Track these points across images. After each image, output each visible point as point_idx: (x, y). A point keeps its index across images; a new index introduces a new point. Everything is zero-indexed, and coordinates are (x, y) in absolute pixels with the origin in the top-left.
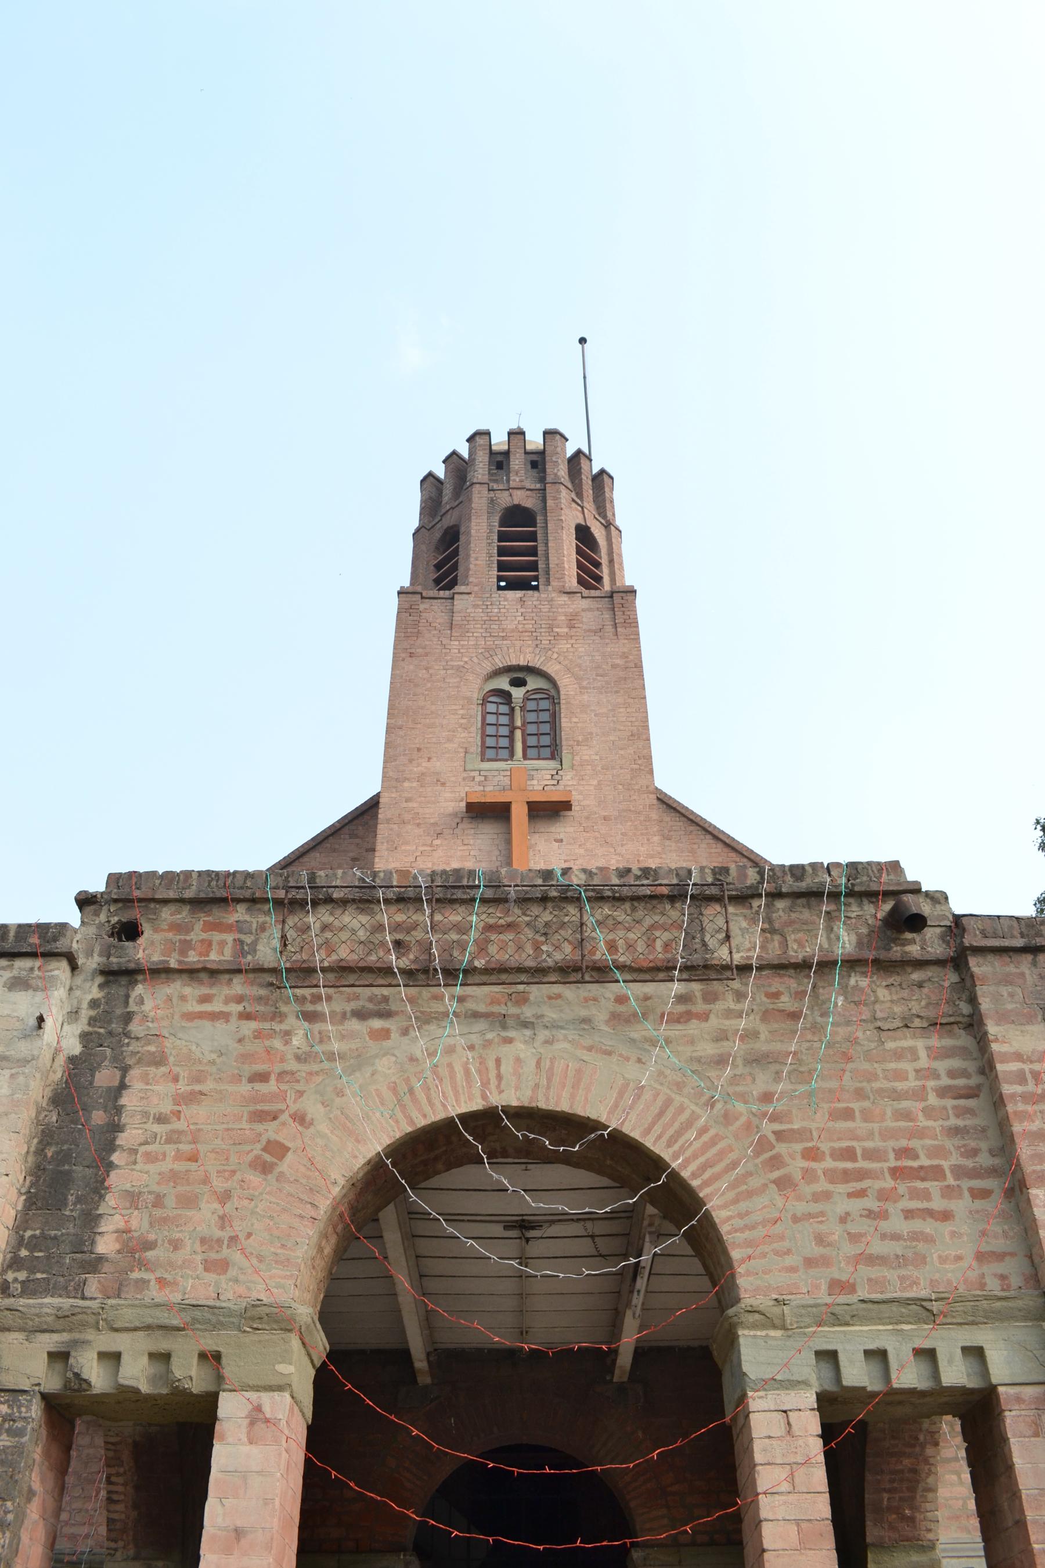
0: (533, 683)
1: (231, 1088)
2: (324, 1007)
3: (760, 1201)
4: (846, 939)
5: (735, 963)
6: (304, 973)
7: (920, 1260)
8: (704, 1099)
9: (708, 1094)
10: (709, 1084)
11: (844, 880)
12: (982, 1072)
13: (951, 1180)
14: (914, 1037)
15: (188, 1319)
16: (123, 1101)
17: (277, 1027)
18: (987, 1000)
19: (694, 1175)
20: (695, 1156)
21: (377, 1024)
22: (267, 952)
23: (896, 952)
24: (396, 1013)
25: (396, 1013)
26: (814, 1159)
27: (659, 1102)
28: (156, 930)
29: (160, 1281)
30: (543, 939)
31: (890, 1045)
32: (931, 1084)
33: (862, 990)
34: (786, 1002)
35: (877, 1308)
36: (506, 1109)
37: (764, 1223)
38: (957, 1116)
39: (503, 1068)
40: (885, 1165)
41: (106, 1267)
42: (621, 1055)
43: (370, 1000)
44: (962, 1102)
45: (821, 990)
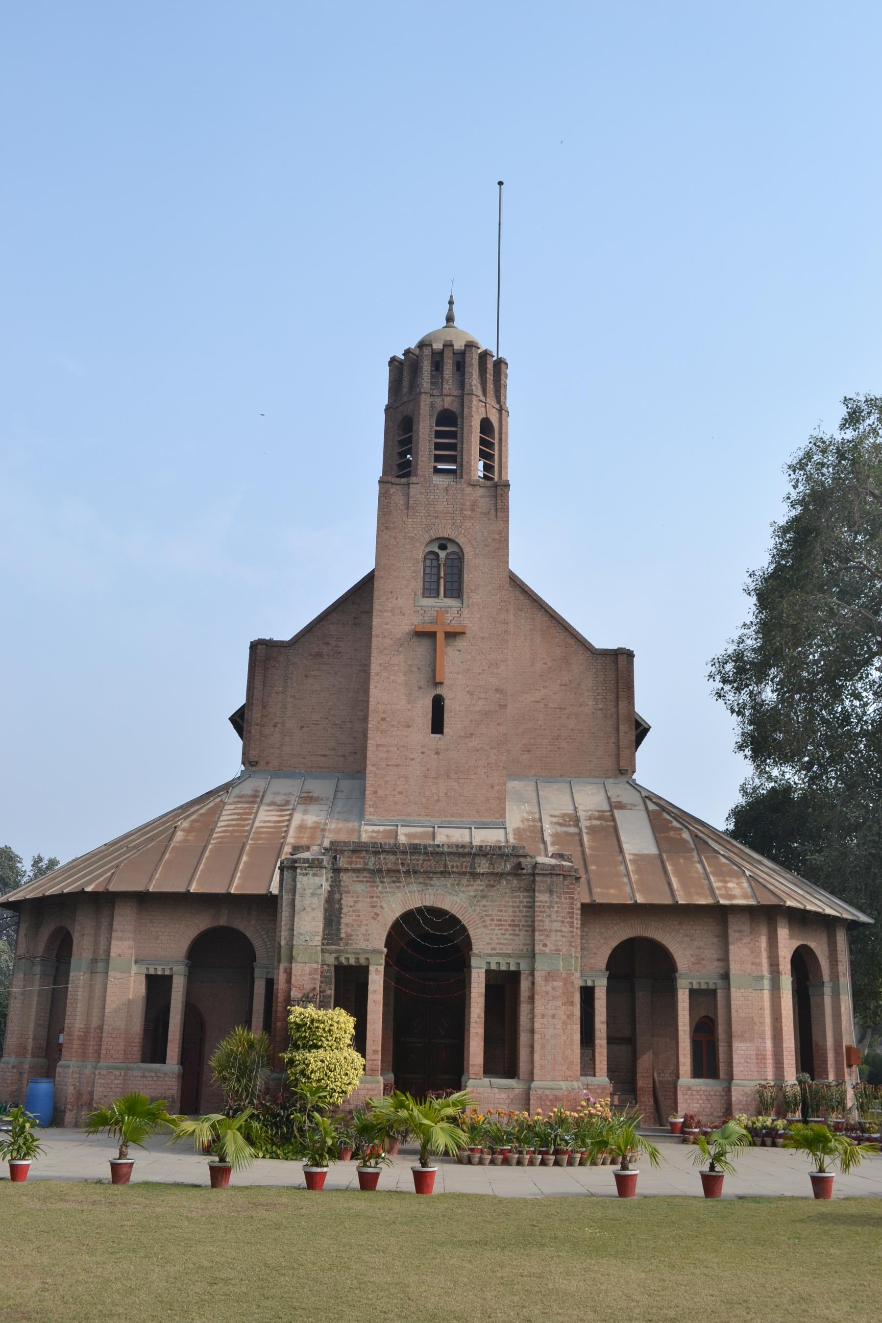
0: (451, 548)
2: (385, 880)
21: (398, 884)
22: (371, 866)
35: (498, 955)
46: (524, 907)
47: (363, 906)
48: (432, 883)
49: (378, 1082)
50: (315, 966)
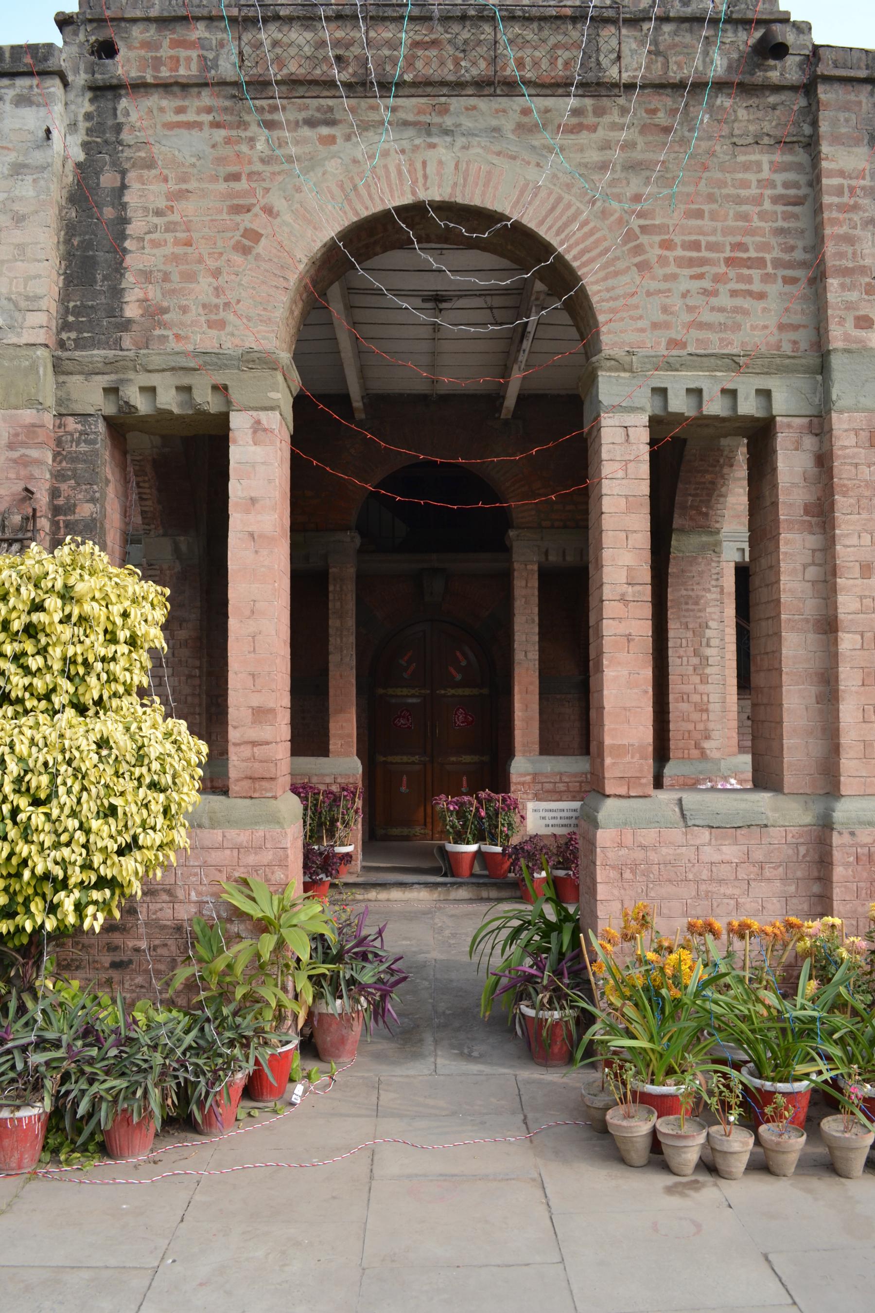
1: (212, 186)
2: (281, 117)
3: (624, 279)
4: (719, 63)
5: (623, 81)
6: (260, 85)
7: (737, 327)
8: (588, 198)
9: (591, 193)
10: (592, 186)
11: (724, 7)
12: (810, 184)
13: (770, 269)
14: (761, 152)
15: (201, 362)
16: (126, 199)
17: (243, 134)
18: (826, 123)
19: (575, 258)
20: (577, 243)
21: (325, 131)
22: (227, 67)
23: (759, 76)
24: (340, 121)
25: (340, 121)
26: (667, 249)
27: (552, 200)
28: (130, 48)
29: (177, 337)
30: (462, 55)
31: (741, 158)
32: (768, 192)
33: (725, 109)
34: (661, 118)
36: (431, 203)
37: (625, 296)
38: (784, 219)
39: (428, 169)
40: (722, 255)
41: (135, 327)
42: (523, 160)
43: (318, 109)
44: (790, 208)
45: (691, 109)
46: (775, 200)
47: (201, 209)
48: (449, 121)
49: (274, 820)
50: (28, 415)
